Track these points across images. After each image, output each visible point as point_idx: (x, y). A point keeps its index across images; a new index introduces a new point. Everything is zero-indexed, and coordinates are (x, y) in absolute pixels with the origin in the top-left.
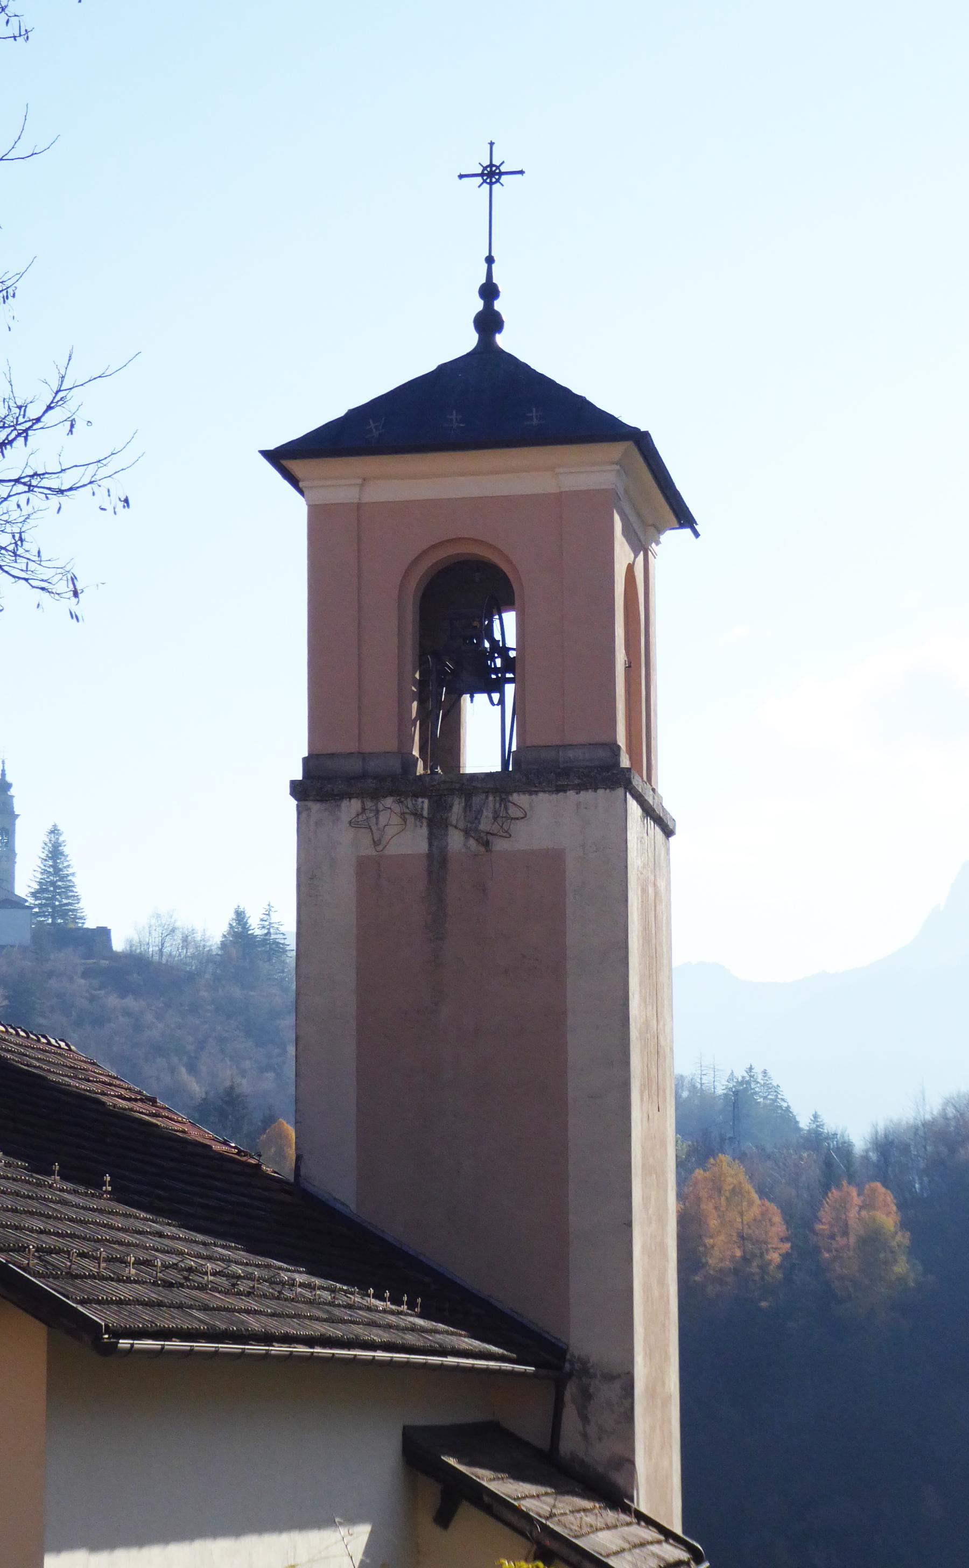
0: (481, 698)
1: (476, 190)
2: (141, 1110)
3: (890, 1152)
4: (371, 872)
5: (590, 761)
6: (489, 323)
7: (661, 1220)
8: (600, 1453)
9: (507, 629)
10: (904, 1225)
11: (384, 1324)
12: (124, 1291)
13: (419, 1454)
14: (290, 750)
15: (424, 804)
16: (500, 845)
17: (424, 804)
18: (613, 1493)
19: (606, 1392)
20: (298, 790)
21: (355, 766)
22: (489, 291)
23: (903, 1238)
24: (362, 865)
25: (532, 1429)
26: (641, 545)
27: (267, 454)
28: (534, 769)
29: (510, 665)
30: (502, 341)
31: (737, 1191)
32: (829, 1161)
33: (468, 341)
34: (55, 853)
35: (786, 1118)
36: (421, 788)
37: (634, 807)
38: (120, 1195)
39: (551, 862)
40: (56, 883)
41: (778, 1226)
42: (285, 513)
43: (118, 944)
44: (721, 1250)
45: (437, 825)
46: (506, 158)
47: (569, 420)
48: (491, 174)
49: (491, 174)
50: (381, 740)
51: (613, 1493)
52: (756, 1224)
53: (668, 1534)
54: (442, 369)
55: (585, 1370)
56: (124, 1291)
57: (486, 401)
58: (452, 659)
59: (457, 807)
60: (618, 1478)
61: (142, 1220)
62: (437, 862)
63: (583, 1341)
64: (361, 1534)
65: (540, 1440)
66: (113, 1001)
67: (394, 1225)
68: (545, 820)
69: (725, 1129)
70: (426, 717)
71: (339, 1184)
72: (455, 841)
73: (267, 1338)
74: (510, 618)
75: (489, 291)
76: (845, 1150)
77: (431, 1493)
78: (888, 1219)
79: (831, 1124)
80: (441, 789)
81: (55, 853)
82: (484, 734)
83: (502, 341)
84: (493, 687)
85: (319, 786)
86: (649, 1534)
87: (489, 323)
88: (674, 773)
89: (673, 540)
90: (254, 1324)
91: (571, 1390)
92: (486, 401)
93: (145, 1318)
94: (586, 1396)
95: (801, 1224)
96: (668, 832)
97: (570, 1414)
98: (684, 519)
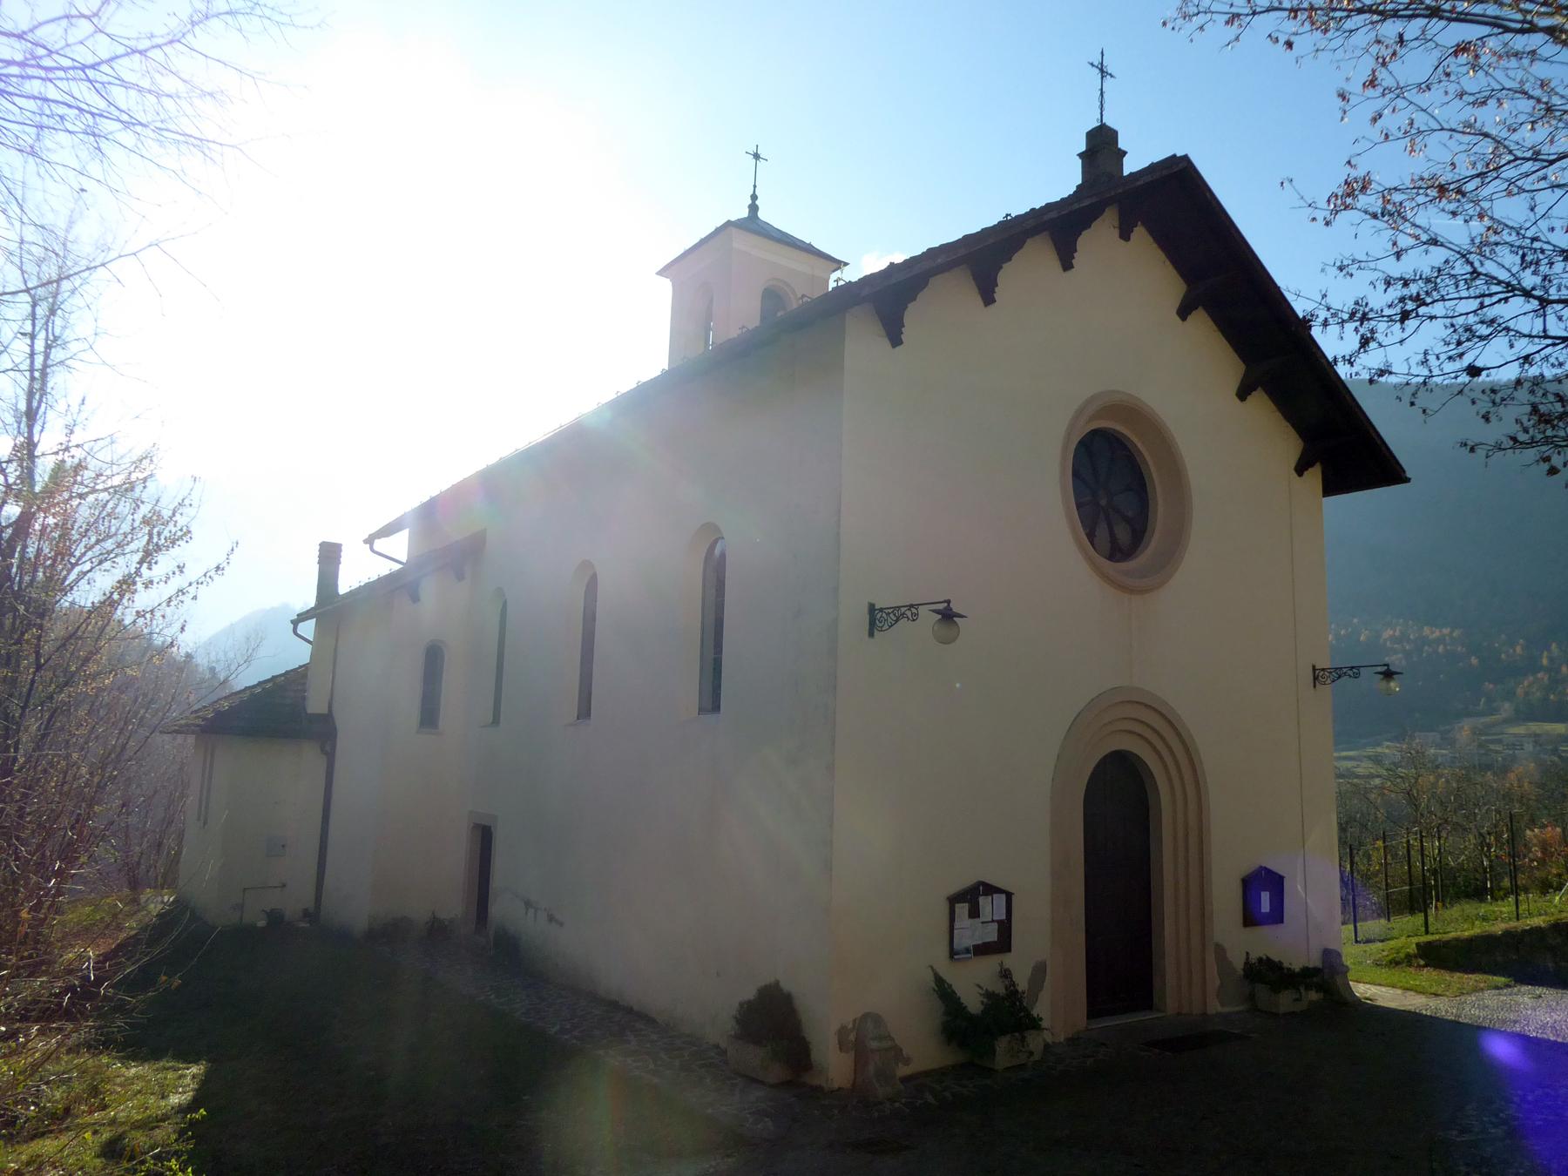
6: (754, 208)
22: (754, 197)
46: (752, 150)
75: (754, 197)
87: (754, 208)
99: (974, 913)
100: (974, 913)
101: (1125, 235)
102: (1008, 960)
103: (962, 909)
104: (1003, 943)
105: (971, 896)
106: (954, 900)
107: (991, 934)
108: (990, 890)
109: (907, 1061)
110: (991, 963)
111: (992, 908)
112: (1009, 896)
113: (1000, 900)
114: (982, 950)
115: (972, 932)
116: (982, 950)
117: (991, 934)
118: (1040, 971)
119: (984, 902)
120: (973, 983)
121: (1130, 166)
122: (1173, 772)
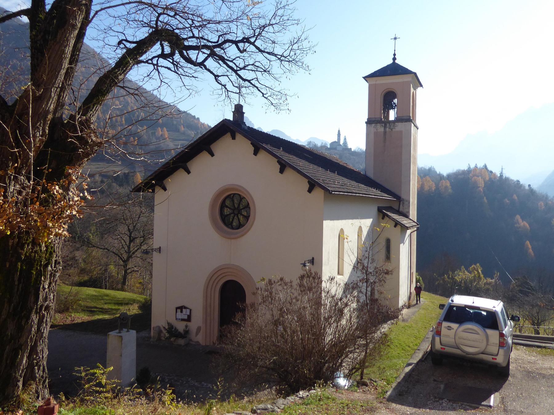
0: (392, 110)
1: (393, 41)
2: (345, 165)
3: (449, 176)
4: (376, 134)
5: (407, 118)
6: (394, 59)
7: (415, 181)
8: (405, 211)
9: (395, 101)
10: (451, 185)
11: (374, 192)
12: (335, 186)
13: (380, 210)
14: (365, 117)
15: (383, 125)
16: (394, 130)
17: (383, 125)
18: (406, 216)
19: (406, 203)
20: (366, 123)
21: (374, 119)
22: (395, 55)
23: (450, 187)
24: (375, 133)
25: (396, 207)
26: (415, 89)
27: (364, 78)
28: (398, 119)
29: (396, 106)
30: (396, 61)
31: (429, 181)
32: (441, 177)
33: (391, 62)
34: (345, 139)
35: (436, 172)
36: (383, 122)
37: (412, 125)
38: (338, 174)
39: (401, 132)
40: (345, 143)
41: (434, 185)
42: (366, 85)
43: (353, 150)
44: (426, 188)
45: (385, 127)
46: (397, 36)
47: (405, 71)
48: (395, 38)
49: (395, 38)
50: (378, 116)
51: (406, 216)
52: (430, 185)
53: (414, 222)
54: (388, 66)
55: (403, 200)
56: (335, 186)
57: (394, 69)
58: (388, 104)
59: (388, 125)
60: (407, 214)
61: (341, 177)
62: (385, 132)
63: (403, 196)
64: (371, 220)
65: (397, 209)
66: (352, 157)
67: (378, 181)
68: (400, 126)
69: (427, 174)
70: (384, 113)
71: (371, 175)
72: (387, 129)
73: (356, 193)
74: (396, 100)
75: (395, 55)
76: (443, 176)
77: (381, 215)
78: (448, 184)
79: (441, 173)
80: (386, 122)
81: (345, 139)
82: (392, 115)
83: (396, 61)
84: (393, 109)
85: (369, 122)
86: (411, 221)
87: (394, 59)
88: (419, 120)
89: (419, 89)
90: (354, 191)
91: (401, 203)
92: (394, 69)
93: (337, 189)
94: (403, 203)
95: (437, 185)
96: (418, 129)
97: (401, 205)
98: (421, 86)
99: (182, 312)
100: (182, 312)
101: (234, 138)
102: (189, 323)
103: (179, 310)
104: (189, 319)
105: (181, 308)
106: (177, 308)
107: (186, 317)
108: (186, 308)
109: (345, 385)
110: (185, 323)
111: (186, 312)
112: (190, 310)
113: (188, 311)
114: (183, 320)
115: (180, 316)
116: (183, 320)
117: (186, 317)
118: (199, 329)
119: (184, 310)
120: (181, 327)
121: (232, 119)
122: (214, 286)
